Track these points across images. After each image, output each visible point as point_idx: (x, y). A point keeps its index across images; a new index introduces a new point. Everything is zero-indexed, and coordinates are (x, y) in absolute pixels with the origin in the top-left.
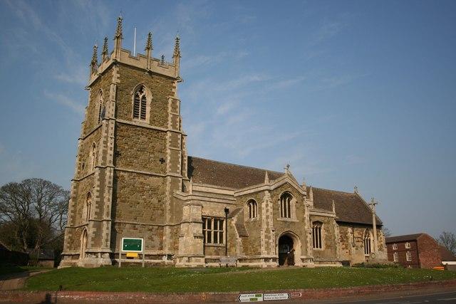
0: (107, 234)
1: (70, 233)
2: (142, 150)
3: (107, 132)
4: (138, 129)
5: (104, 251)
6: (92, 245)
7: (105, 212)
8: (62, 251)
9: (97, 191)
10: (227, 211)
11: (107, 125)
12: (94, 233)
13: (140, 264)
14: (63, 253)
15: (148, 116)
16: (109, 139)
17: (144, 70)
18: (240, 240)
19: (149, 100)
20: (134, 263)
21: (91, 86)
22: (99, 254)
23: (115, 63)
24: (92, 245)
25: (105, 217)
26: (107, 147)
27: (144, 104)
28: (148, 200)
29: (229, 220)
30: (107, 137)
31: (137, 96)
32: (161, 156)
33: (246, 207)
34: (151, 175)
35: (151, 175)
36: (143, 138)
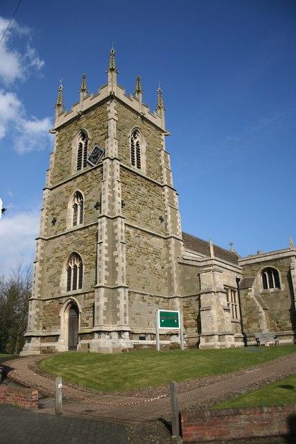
0: (125, 306)
1: (37, 306)
2: (144, 203)
3: (112, 174)
4: (138, 177)
5: (124, 329)
6: (104, 321)
7: (119, 277)
8: (25, 330)
9: (106, 248)
10: (238, 280)
11: (112, 166)
12: (106, 304)
13: (154, 346)
14: (27, 334)
15: (143, 165)
16: (116, 182)
17: (137, 114)
18: (263, 313)
19: (143, 147)
20: (148, 345)
21: (58, 129)
22: (217, 337)
23: (112, 97)
24: (104, 321)
25: (119, 283)
26: (113, 192)
27: (138, 150)
28: (153, 265)
29: (242, 292)
30: (113, 181)
31: (132, 141)
32: (160, 214)
33: (260, 277)
34: (154, 235)
35: (154, 235)
36: (144, 190)
